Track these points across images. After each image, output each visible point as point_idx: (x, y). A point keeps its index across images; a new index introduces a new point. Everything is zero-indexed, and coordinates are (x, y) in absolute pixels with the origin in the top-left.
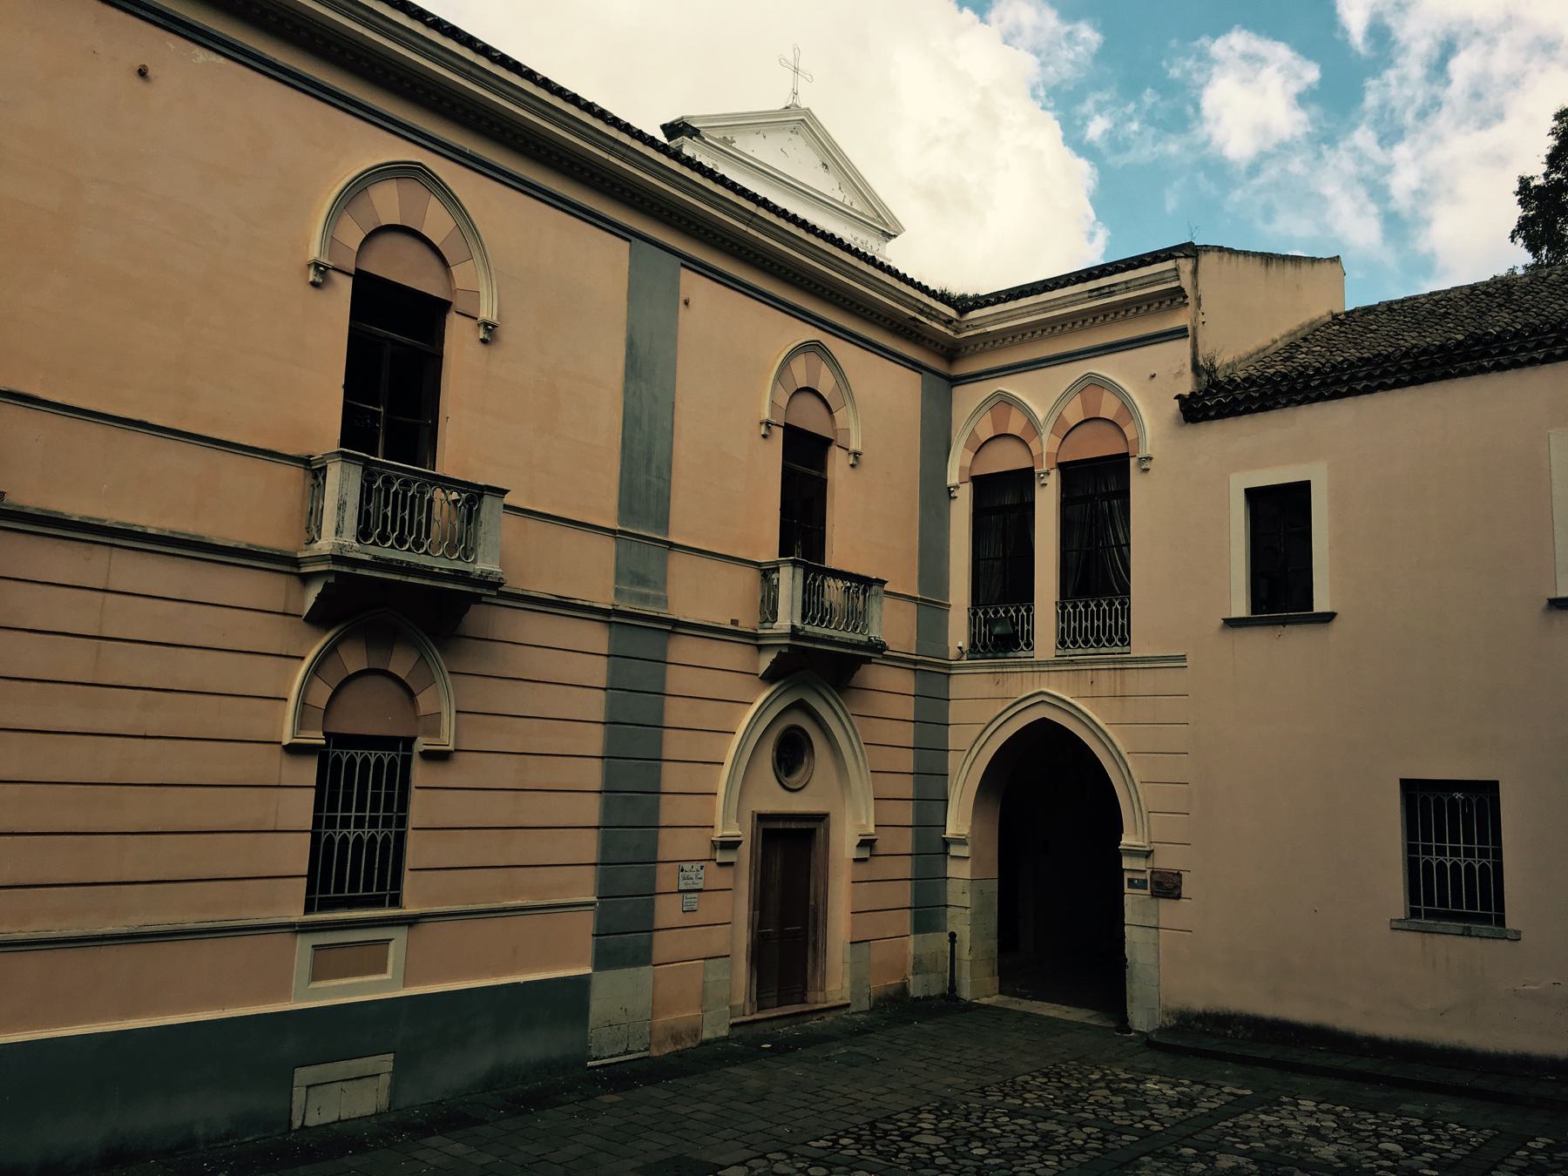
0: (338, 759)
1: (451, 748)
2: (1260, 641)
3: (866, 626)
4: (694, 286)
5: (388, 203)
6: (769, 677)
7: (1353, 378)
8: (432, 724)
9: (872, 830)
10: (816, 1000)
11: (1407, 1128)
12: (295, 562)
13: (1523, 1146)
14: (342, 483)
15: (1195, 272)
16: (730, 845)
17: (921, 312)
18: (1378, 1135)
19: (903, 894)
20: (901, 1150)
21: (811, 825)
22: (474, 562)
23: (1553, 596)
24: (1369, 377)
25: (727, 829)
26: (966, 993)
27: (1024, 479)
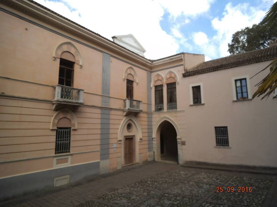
0: (59, 131)
1: (77, 128)
2: (240, 104)
3: (139, 108)
4: (113, 59)
5: (65, 48)
6: (126, 115)
7: (205, 71)
8: (74, 125)
9: (141, 137)
10: (134, 162)
11: (217, 176)
12: (51, 102)
13: (232, 178)
14: (58, 90)
15: (184, 56)
16: (120, 141)
17: (146, 62)
18: (213, 177)
19: (147, 146)
20: (145, 184)
21: (132, 137)
22: (79, 101)
23: (190, 104)
24: (207, 70)
25: (119, 139)
26: (156, 160)
27: (162, 86)
